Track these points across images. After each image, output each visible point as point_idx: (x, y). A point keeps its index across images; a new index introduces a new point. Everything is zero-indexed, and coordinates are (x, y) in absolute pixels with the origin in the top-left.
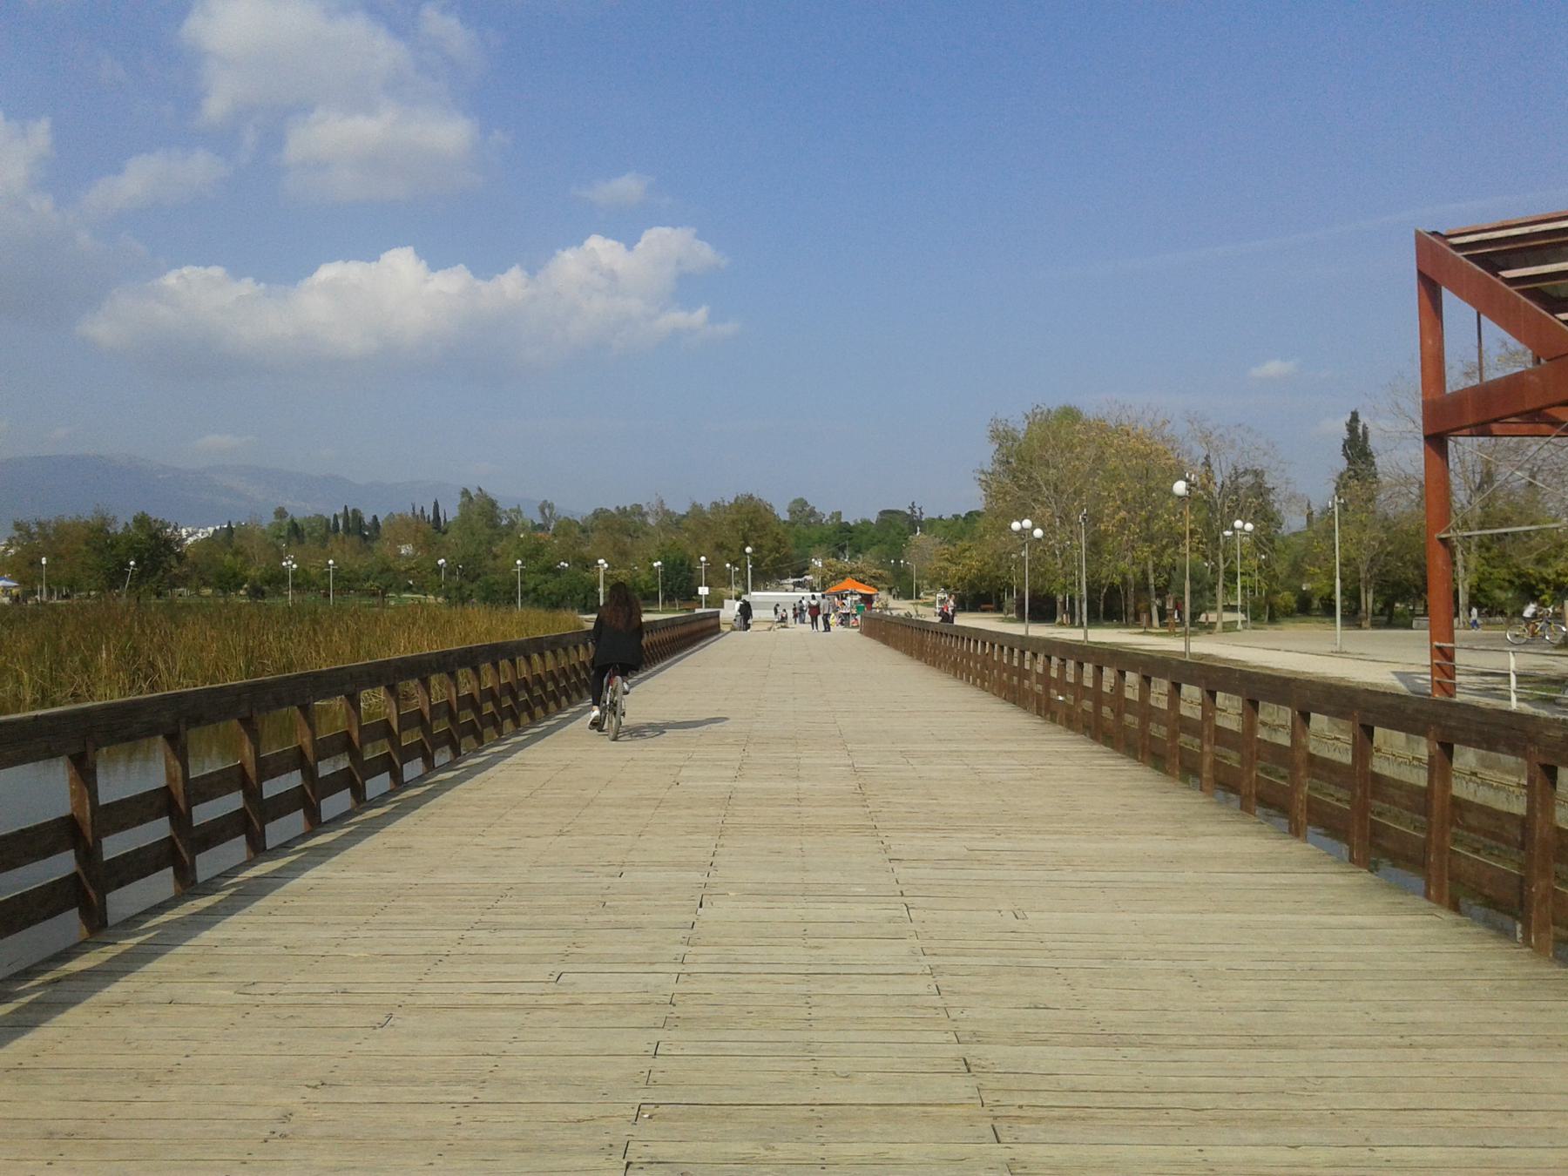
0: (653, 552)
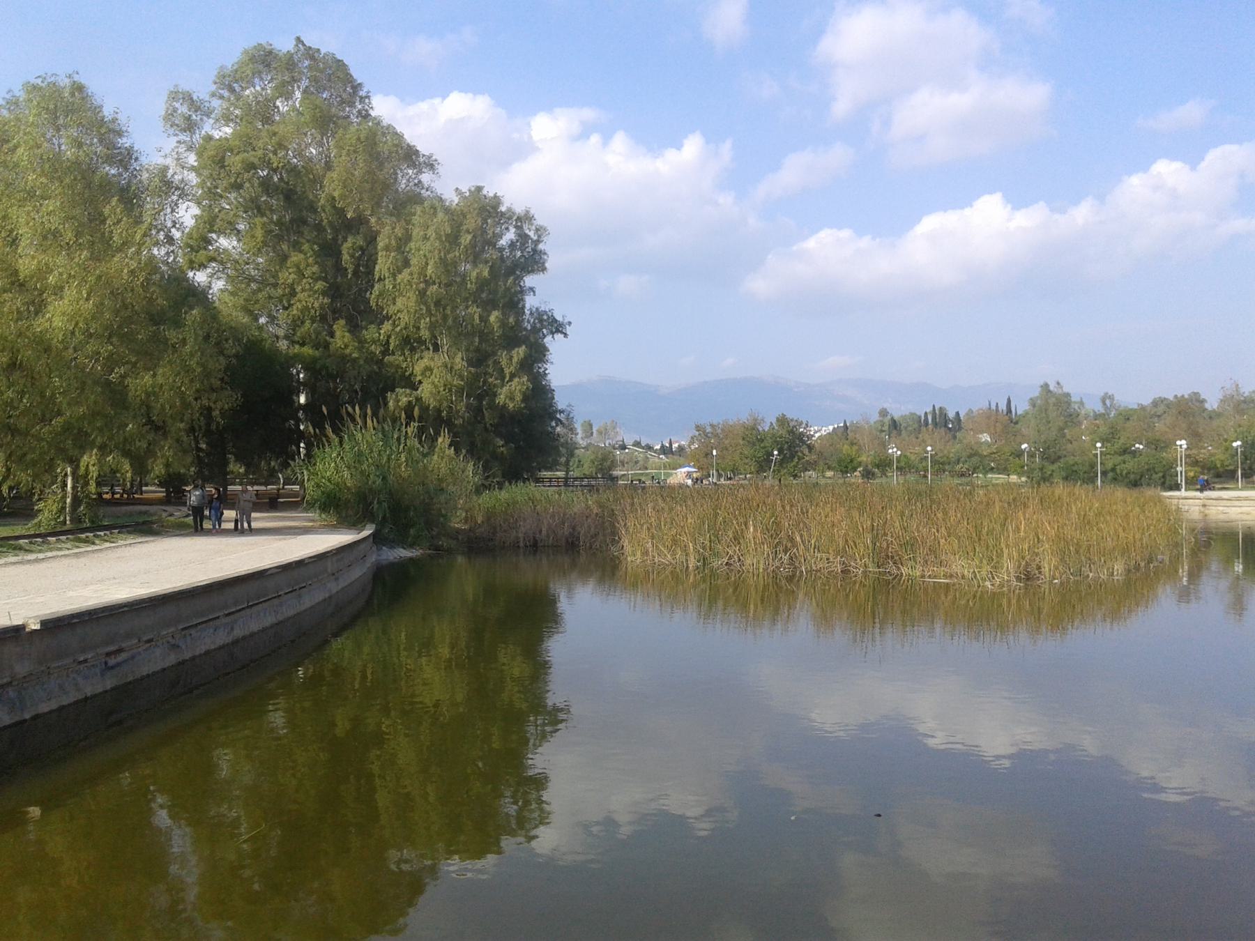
0: (1232, 434)
